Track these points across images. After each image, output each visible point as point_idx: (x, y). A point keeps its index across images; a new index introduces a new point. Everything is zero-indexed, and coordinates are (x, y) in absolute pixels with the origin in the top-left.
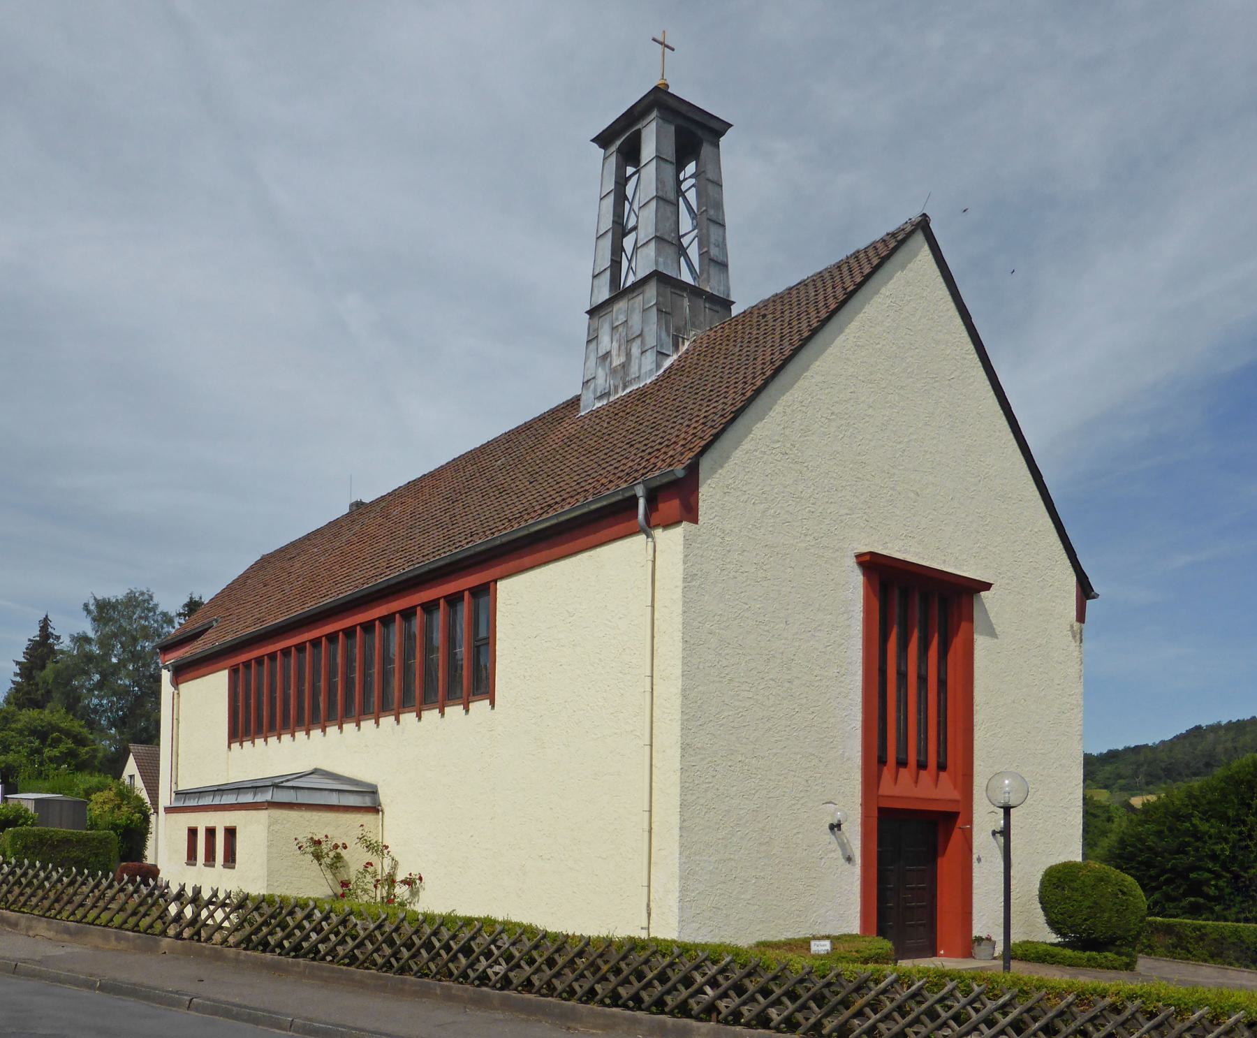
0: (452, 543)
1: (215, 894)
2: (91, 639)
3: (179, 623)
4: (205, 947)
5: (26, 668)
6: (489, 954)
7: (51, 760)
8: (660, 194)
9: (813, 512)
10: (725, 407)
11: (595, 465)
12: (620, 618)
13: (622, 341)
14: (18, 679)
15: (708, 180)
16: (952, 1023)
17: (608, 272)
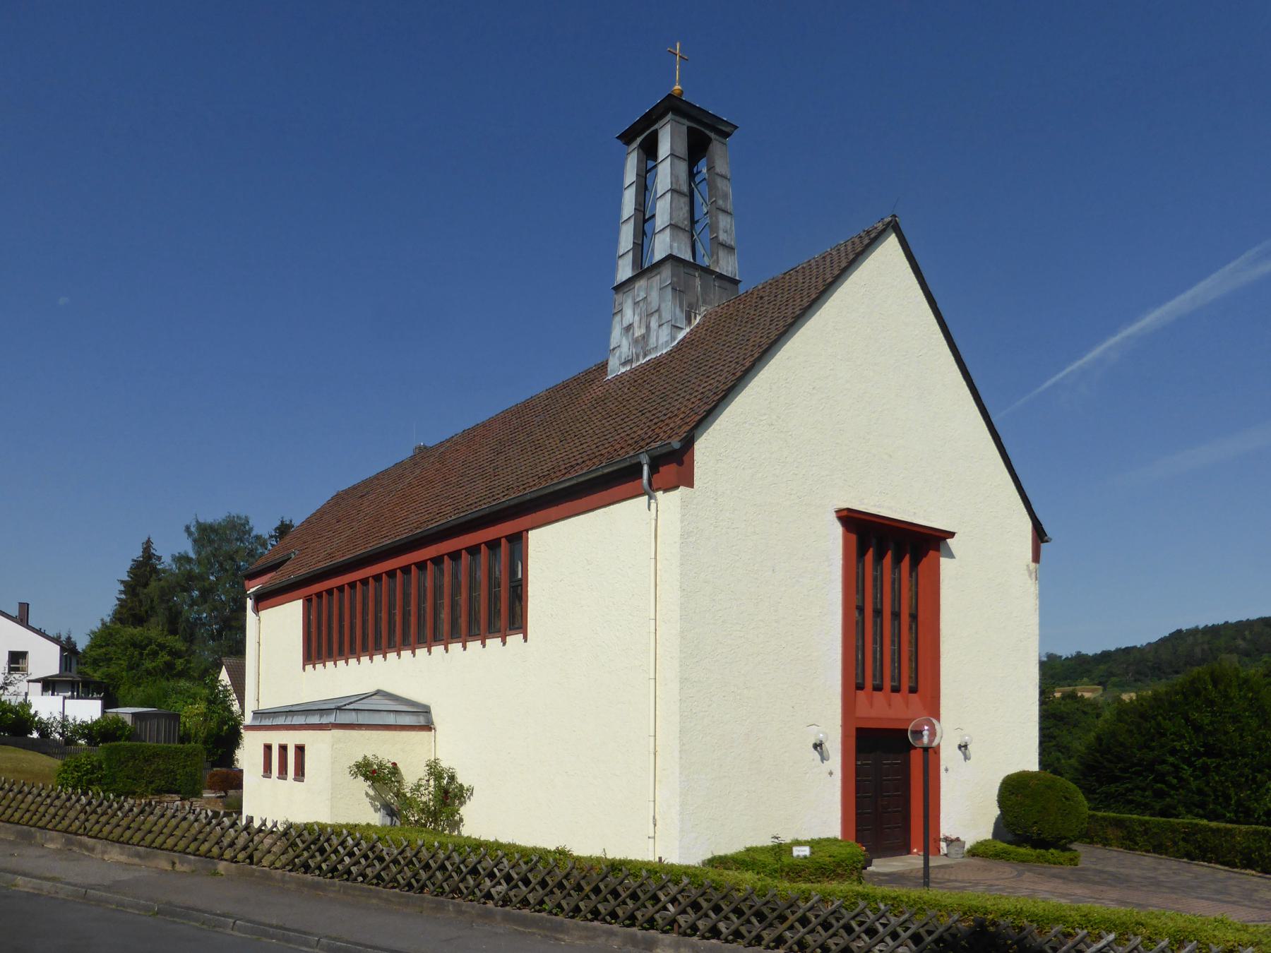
0: (491, 494)
1: (264, 824)
2: (192, 559)
3: (271, 544)
4: (255, 870)
5: (130, 586)
6: (491, 875)
7: (149, 673)
8: (674, 187)
9: (796, 475)
10: (719, 385)
11: (613, 430)
12: (630, 568)
13: (643, 315)
14: (123, 596)
15: (717, 174)
16: (864, 936)
17: (631, 253)
